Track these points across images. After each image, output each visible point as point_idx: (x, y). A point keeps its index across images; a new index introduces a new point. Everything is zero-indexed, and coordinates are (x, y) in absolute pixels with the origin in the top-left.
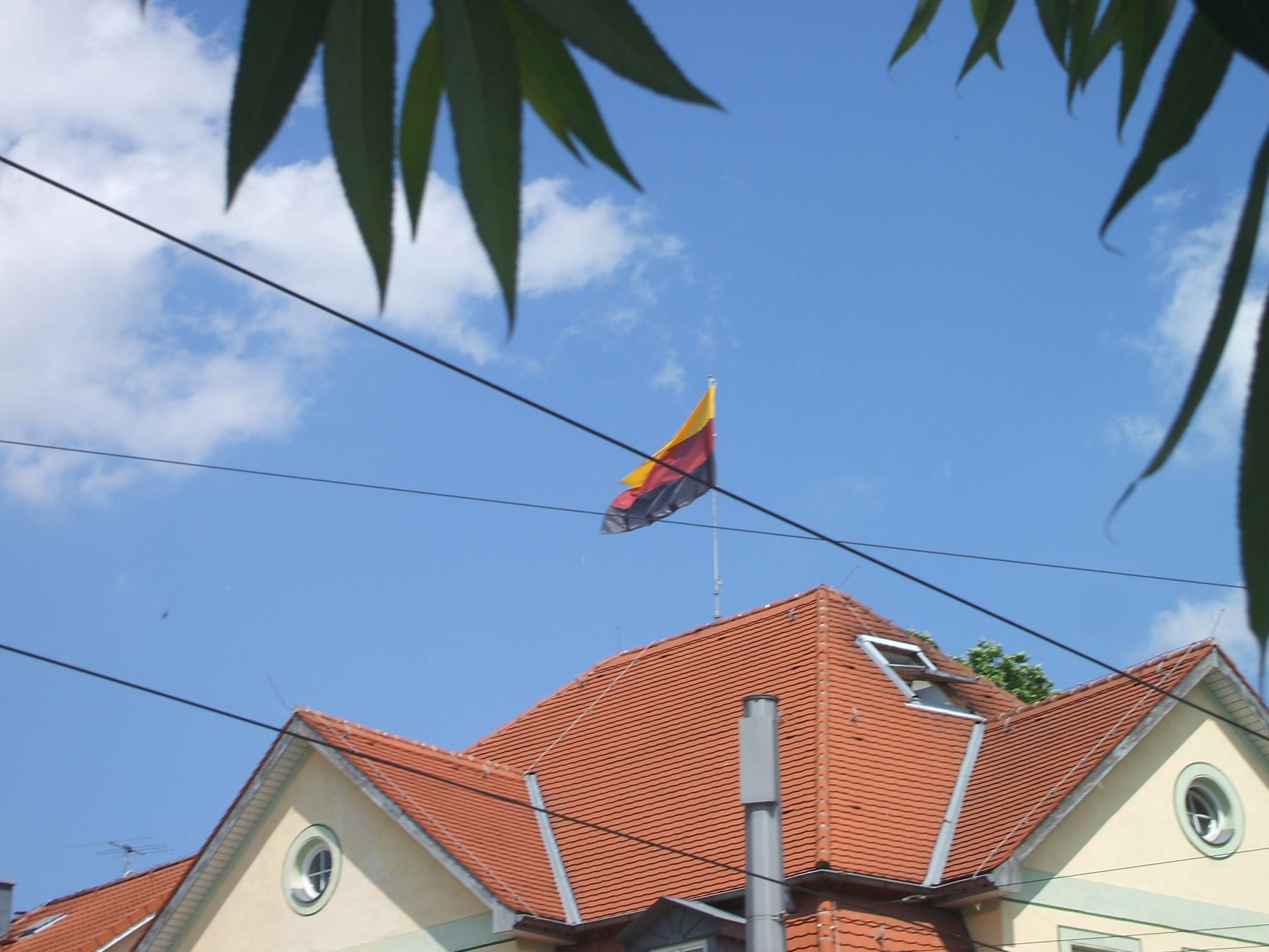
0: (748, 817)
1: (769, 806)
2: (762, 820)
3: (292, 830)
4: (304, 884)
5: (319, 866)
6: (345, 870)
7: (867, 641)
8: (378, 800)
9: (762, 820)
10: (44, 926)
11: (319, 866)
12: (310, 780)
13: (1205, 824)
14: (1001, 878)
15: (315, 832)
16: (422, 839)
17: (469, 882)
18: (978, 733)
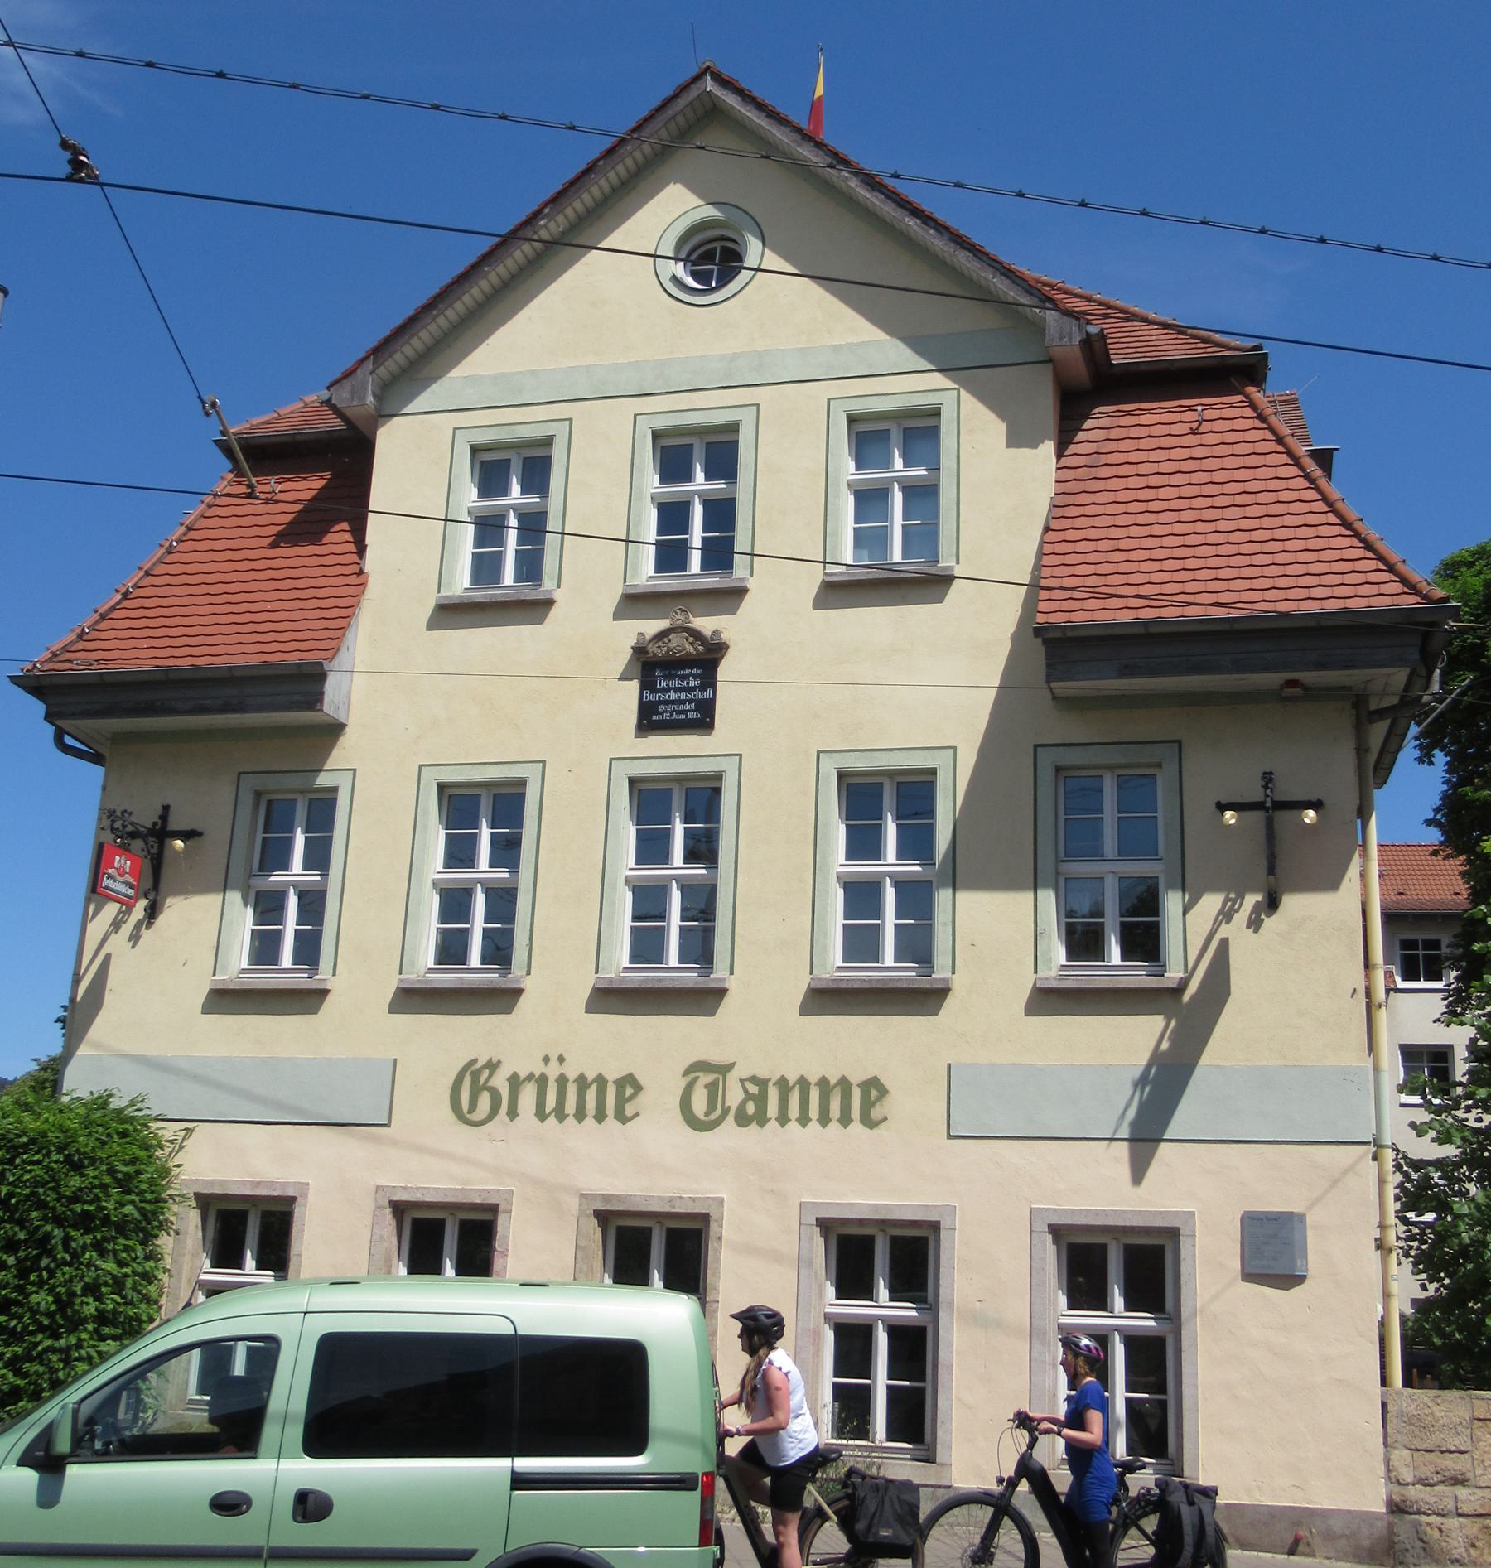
3: (671, 210)
15: (711, 212)
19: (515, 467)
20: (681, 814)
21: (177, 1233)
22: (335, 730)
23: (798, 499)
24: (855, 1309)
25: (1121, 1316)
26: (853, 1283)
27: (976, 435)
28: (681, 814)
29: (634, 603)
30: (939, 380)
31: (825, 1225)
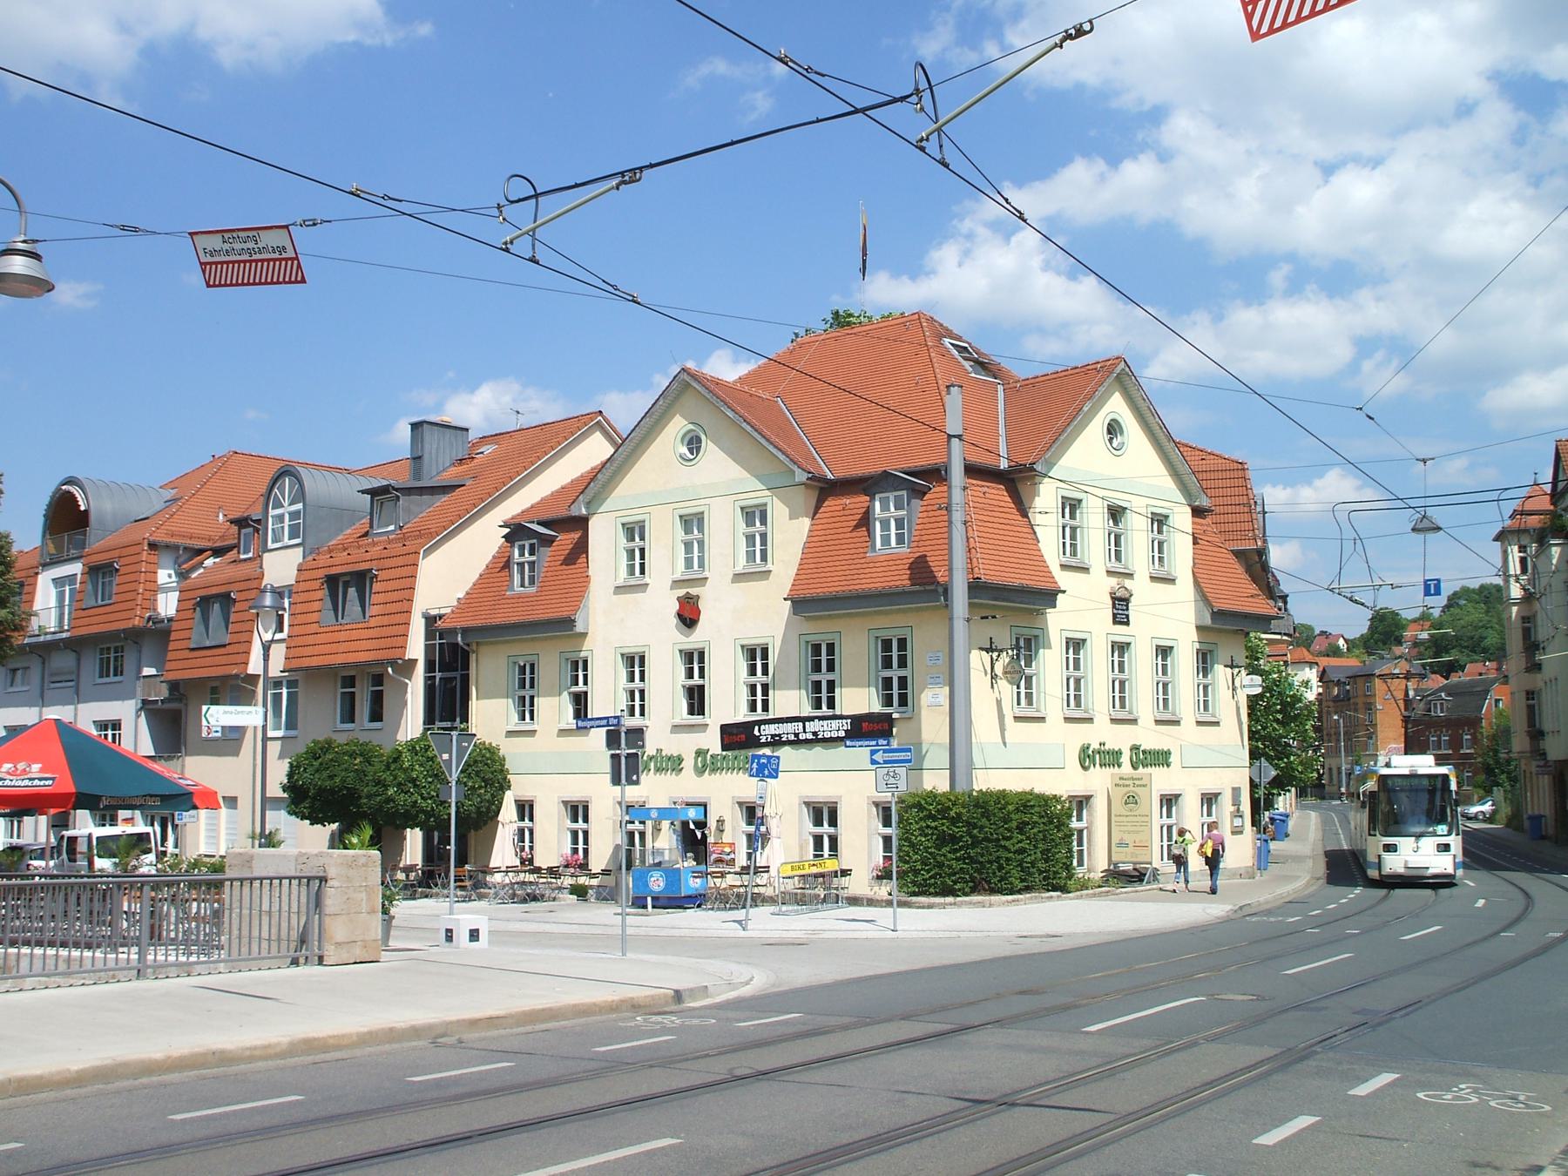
0: (949, 441)
1: (959, 437)
2: (955, 441)
3: (677, 426)
4: (684, 450)
5: (694, 444)
6: (708, 446)
7: (947, 341)
8: (730, 414)
9: (955, 441)
10: (488, 449)
11: (694, 444)
12: (688, 400)
13: (1111, 440)
14: (1038, 467)
15: (691, 427)
16: (756, 435)
17: (782, 457)
18: (1000, 388)
19: (634, 530)
20: (694, 659)
21: (1513, 780)
22: (584, 635)
23: (725, 540)
24: (818, 830)
25: (826, 829)
26: (818, 822)
27: (778, 511)
28: (694, 659)
29: (677, 584)
30: (767, 493)
31: (807, 804)
